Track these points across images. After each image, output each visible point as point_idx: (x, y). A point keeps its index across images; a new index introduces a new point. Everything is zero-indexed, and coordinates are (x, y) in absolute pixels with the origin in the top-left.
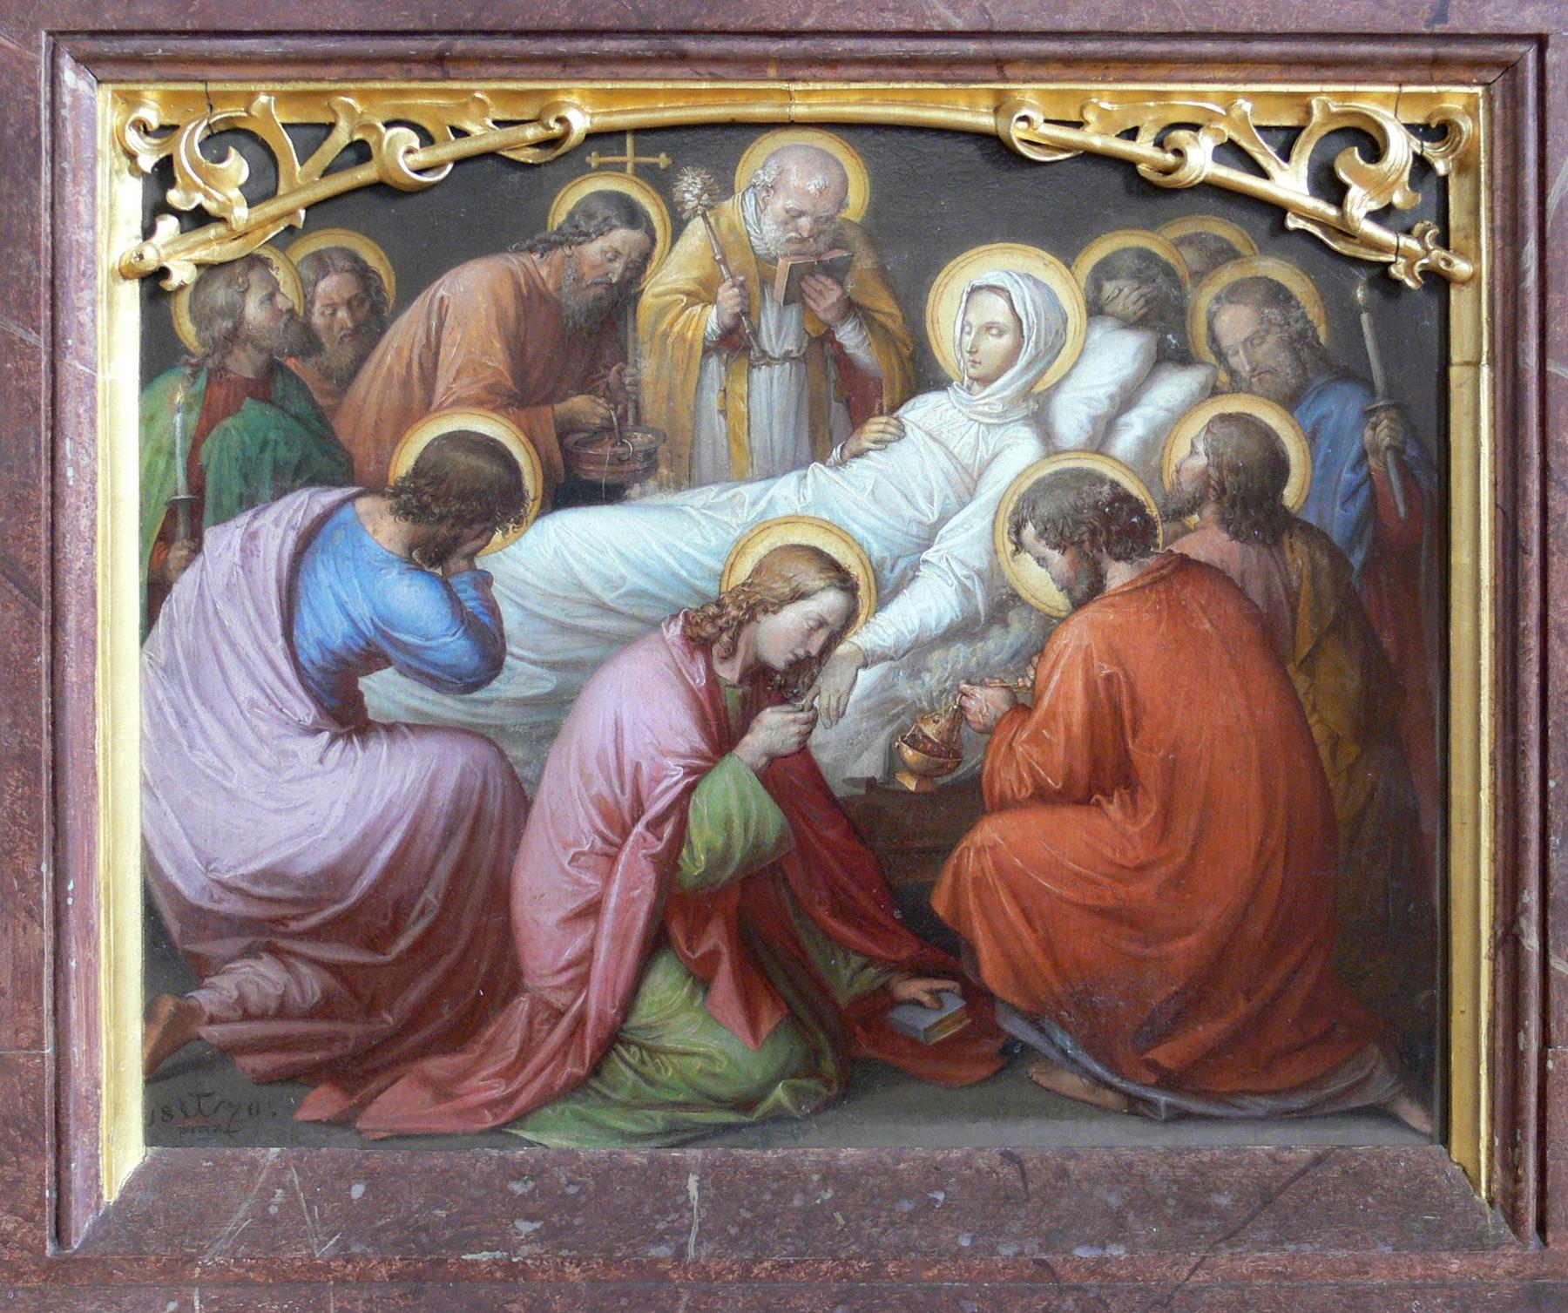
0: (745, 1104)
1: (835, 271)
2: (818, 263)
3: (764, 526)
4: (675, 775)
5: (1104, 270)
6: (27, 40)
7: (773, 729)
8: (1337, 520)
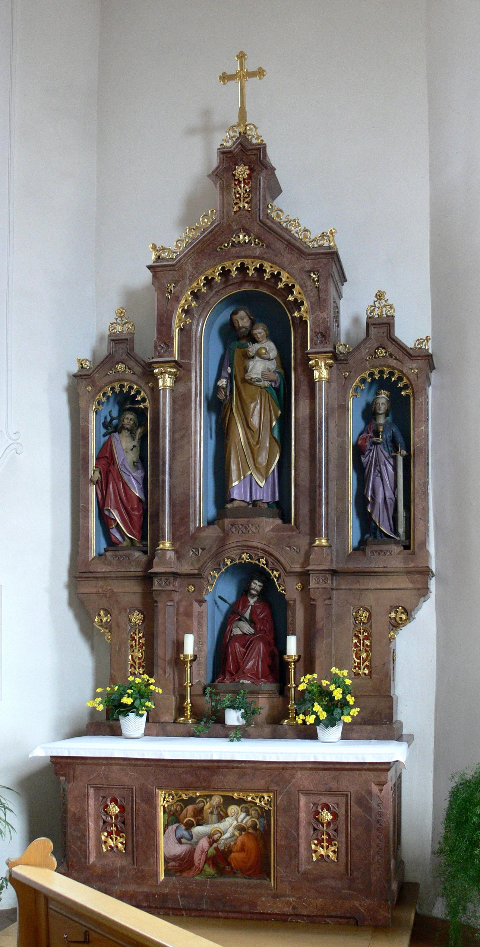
0: (213, 876)
1: (220, 807)
2: (218, 806)
3: (214, 828)
4: (207, 849)
5: (242, 808)
6: (153, 787)
7: (215, 845)
8: (262, 829)
